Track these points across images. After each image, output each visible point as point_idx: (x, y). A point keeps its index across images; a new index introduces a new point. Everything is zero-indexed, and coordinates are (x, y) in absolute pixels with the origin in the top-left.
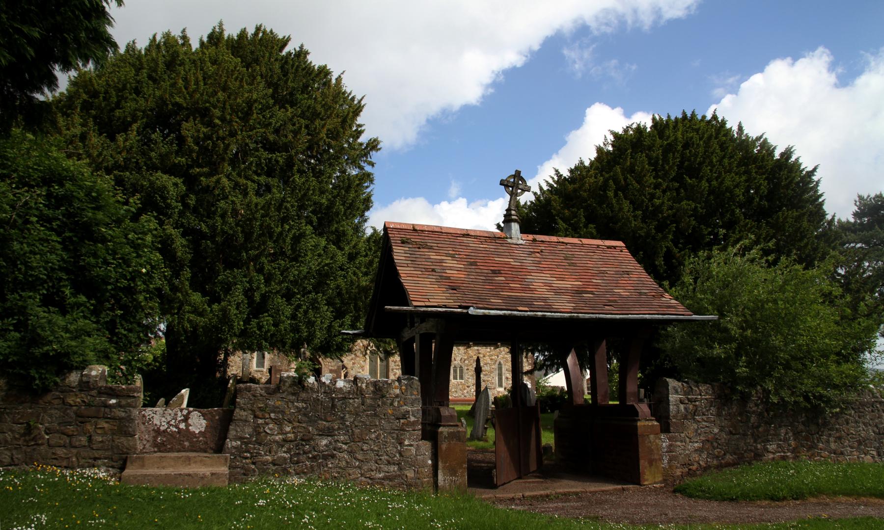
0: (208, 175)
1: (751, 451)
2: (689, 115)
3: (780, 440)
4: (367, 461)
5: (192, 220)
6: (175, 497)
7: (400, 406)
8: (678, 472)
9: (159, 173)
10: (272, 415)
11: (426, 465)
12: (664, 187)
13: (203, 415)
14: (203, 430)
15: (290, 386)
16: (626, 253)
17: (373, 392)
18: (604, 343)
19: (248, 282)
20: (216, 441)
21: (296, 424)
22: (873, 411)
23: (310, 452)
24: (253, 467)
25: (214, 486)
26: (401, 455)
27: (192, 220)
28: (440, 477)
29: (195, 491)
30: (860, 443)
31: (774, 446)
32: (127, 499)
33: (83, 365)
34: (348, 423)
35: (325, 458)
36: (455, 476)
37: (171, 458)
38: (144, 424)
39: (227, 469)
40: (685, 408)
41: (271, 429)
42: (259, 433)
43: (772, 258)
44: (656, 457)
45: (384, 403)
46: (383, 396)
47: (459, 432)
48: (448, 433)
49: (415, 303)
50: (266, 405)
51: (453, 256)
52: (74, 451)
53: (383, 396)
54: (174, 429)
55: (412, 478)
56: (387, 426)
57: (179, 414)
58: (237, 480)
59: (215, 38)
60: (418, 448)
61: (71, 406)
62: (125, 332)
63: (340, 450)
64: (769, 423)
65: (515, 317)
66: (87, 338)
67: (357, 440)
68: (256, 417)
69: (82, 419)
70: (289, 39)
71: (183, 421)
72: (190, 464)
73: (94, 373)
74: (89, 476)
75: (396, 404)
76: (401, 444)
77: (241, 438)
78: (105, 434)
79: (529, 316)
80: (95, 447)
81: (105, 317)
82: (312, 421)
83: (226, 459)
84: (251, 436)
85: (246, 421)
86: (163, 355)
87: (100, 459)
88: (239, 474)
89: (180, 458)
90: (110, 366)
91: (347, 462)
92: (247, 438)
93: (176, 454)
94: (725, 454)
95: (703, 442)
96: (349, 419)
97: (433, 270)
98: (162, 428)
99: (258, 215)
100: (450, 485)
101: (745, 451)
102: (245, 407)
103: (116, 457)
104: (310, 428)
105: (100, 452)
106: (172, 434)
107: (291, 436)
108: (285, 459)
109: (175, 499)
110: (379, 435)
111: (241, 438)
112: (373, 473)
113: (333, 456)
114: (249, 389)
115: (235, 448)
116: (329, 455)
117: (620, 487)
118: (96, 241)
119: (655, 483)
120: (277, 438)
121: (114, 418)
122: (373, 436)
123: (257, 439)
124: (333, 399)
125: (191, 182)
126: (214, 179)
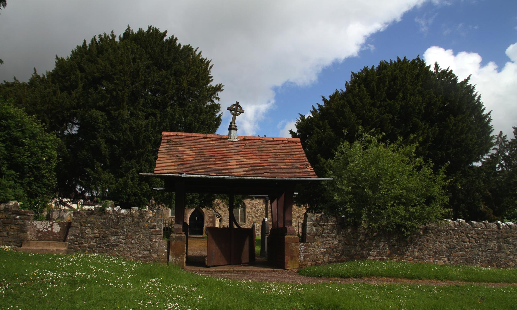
0: (115, 110)
1: (359, 254)
2: (402, 60)
3: (379, 249)
4: (134, 248)
7: (151, 222)
8: (309, 264)
9: (94, 110)
10: (89, 225)
11: (163, 252)
12: (378, 105)
15: (98, 212)
16: (300, 145)
17: (139, 215)
19: (139, 166)
22: (446, 235)
23: (106, 243)
28: (170, 258)
30: (435, 253)
31: (375, 253)
35: (113, 246)
40: (316, 230)
41: (88, 231)
42: (82, 233)
43: (100, 146)
44: (295, 255)
45: (143, 221)
46: (143, 218)
49: (155, 172)
51: (191, 149)
53: (143, 218)
55: (156, 258)
56: (145, 232)
59: (127, 34)
60: (160, 243)
63: (121, 242)
64: (372, 239)
65: (207, 178)
68: (82, 226)
70: (166, 32)
71: (50, 227)
73: (11, 204)
75: (149, 221)
76: (151, 241)
78: (14, 231)
79: (215, 178)
80: (10, 237)
81: (26, 180)
82: (107, 228)
83: (66, 244)
84: (79, 234)
85: (77, 227)
94: (341, 256)
96: (126, 228)
97: (177, 156)
99: (142, 131)
100: (175, 262)
101: (355, 255)
106: (45, 233)
107: (97, 235)
108: (94, 245)
110: (140, 236)
111: (74, 235)
113: (117, 245)
116: (115, 245)
118: (19, 145)
121: (18, 224)
124: (118, 218)
125: (108, 113)
126: (117, 112)
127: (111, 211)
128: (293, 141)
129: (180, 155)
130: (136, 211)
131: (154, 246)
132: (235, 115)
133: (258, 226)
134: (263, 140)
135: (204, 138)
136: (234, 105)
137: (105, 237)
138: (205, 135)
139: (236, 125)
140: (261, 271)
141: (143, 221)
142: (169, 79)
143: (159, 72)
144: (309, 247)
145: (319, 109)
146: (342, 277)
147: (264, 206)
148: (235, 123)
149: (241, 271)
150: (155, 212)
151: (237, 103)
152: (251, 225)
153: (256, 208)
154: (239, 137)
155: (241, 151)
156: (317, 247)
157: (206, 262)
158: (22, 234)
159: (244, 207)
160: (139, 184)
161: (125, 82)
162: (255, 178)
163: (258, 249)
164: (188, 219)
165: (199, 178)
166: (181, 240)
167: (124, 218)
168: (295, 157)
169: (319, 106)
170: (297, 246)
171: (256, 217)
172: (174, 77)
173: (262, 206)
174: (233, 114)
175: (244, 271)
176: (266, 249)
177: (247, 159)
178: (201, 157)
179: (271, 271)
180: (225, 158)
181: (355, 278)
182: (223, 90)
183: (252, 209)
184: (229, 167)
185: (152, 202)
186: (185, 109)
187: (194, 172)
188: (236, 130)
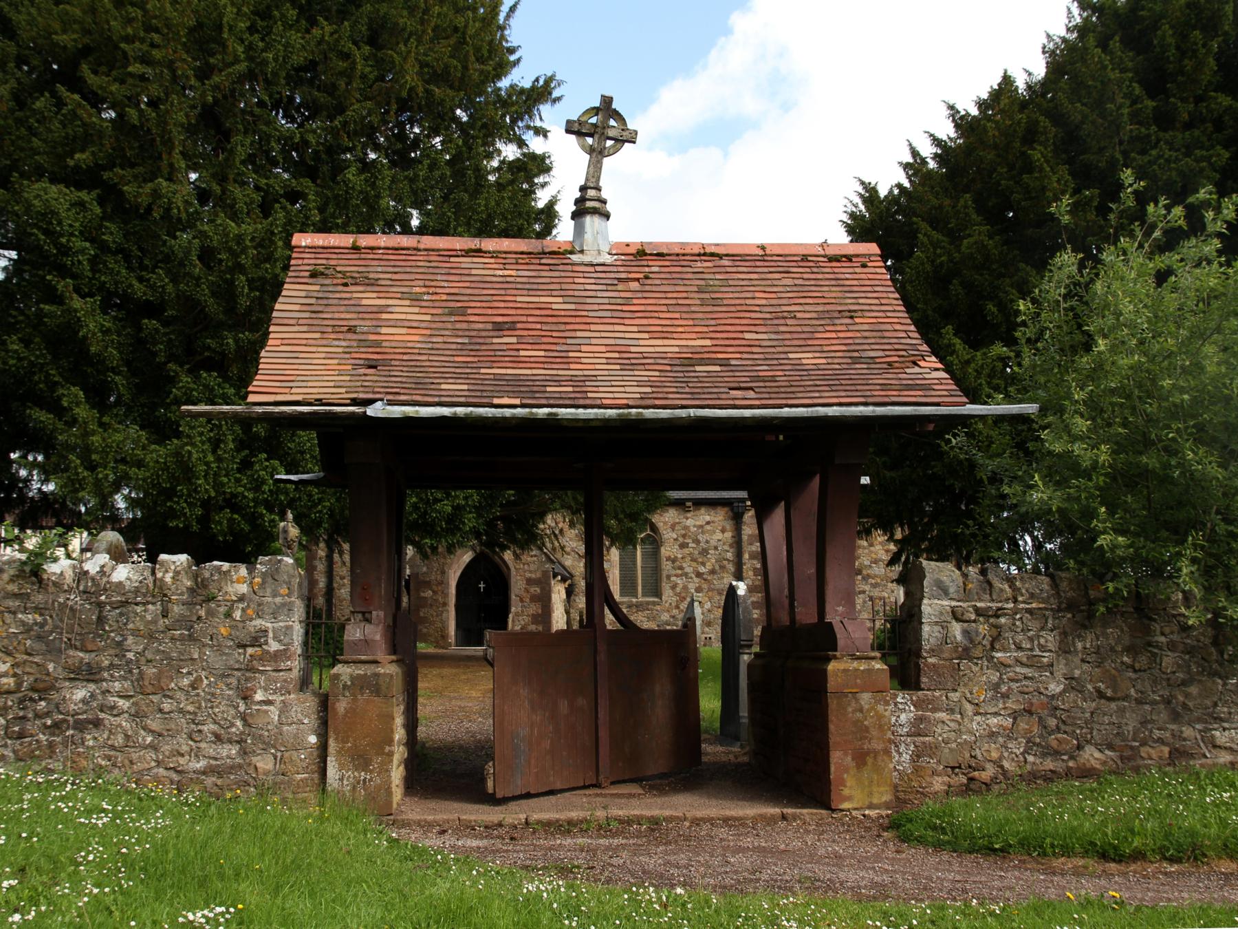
5: (119, 273)
8: (938, 784)
15: (12, 581)
16: (880, 272)
17: (191, 591)
18: (816, 481)
21: (21, 657)
23: (48, 714)
26: (246, 724)
27: (119, 273)
28: (332, 772)
34: (130, 655)
35: (80, 726)
36: (366, 769)
40: (966, 633)
44: (877, 745)
45: (211, 613)
47: (377, 675)
48: (352, 678)
49: (252, 398)
51: (415, 299)
55: (267, 773)
56: (218, 662)
67: (150, 689)
75: (237, 615)
82: (53, 651)
91: (127, 737)
95: (1015, 715)
97: (351, 330)
104: (51, 667)
110: (199, 679)
112: (182, 761)
113: (97, 723)
116: (88, 721)
117: (774, 811)
119: (871, 807)
122: (186, 682)
124: (100, 605)
125: (111, 196)
127: (69, 575)
128: (849, 258)
129: (364, 325)
130: (177, 573)
131: (259, 721)
132: (597, 155)
133: (706, 613)
134: (720, 257)
135: (468, 253)
136: (595, 111)
137: (43, 688)
138: (474, 243)
139: (604, 194)
140: (726, 820)
141: (211, 613)
142: (346, 56)
143: (308, 31)
144: (934, 710)
145: (936, 156)
146: (1104, 856)
147: (729, 535)
148: (599, 189)
149: (639, 820)
150: (264, 575)
151: (607, 101)
152: (684, 606)
153: (697, 542)
154: (617, 245)
155: (627, 301)
156: (969, 708)
157: (490, 784)
159: (655, 542)
160: (246, 465)
161: (171, 65)
162: (692, 412)
163: (710, 703)
164: (453, 590)
165: (443, 418)
166: (377, 691)
167: (125, 603)
168: (863, 323)
169: (937, 142)
170: (880, 708)
171: (699, 575)
172: (367, 49)
173: (719, 536)
174: (591, 151)
175: (655, 822)
176: (744, 712)
177: (653, 335)
178: (456, 333)
179: (770, 821)
180: (557, 332)
181: (1172, 860)
182: (559, 99)
183: (683, 546)
184: (575, 371)
185: (285, 531)
186: (416, 175)
187: (422, 389)
188: (607, 216)
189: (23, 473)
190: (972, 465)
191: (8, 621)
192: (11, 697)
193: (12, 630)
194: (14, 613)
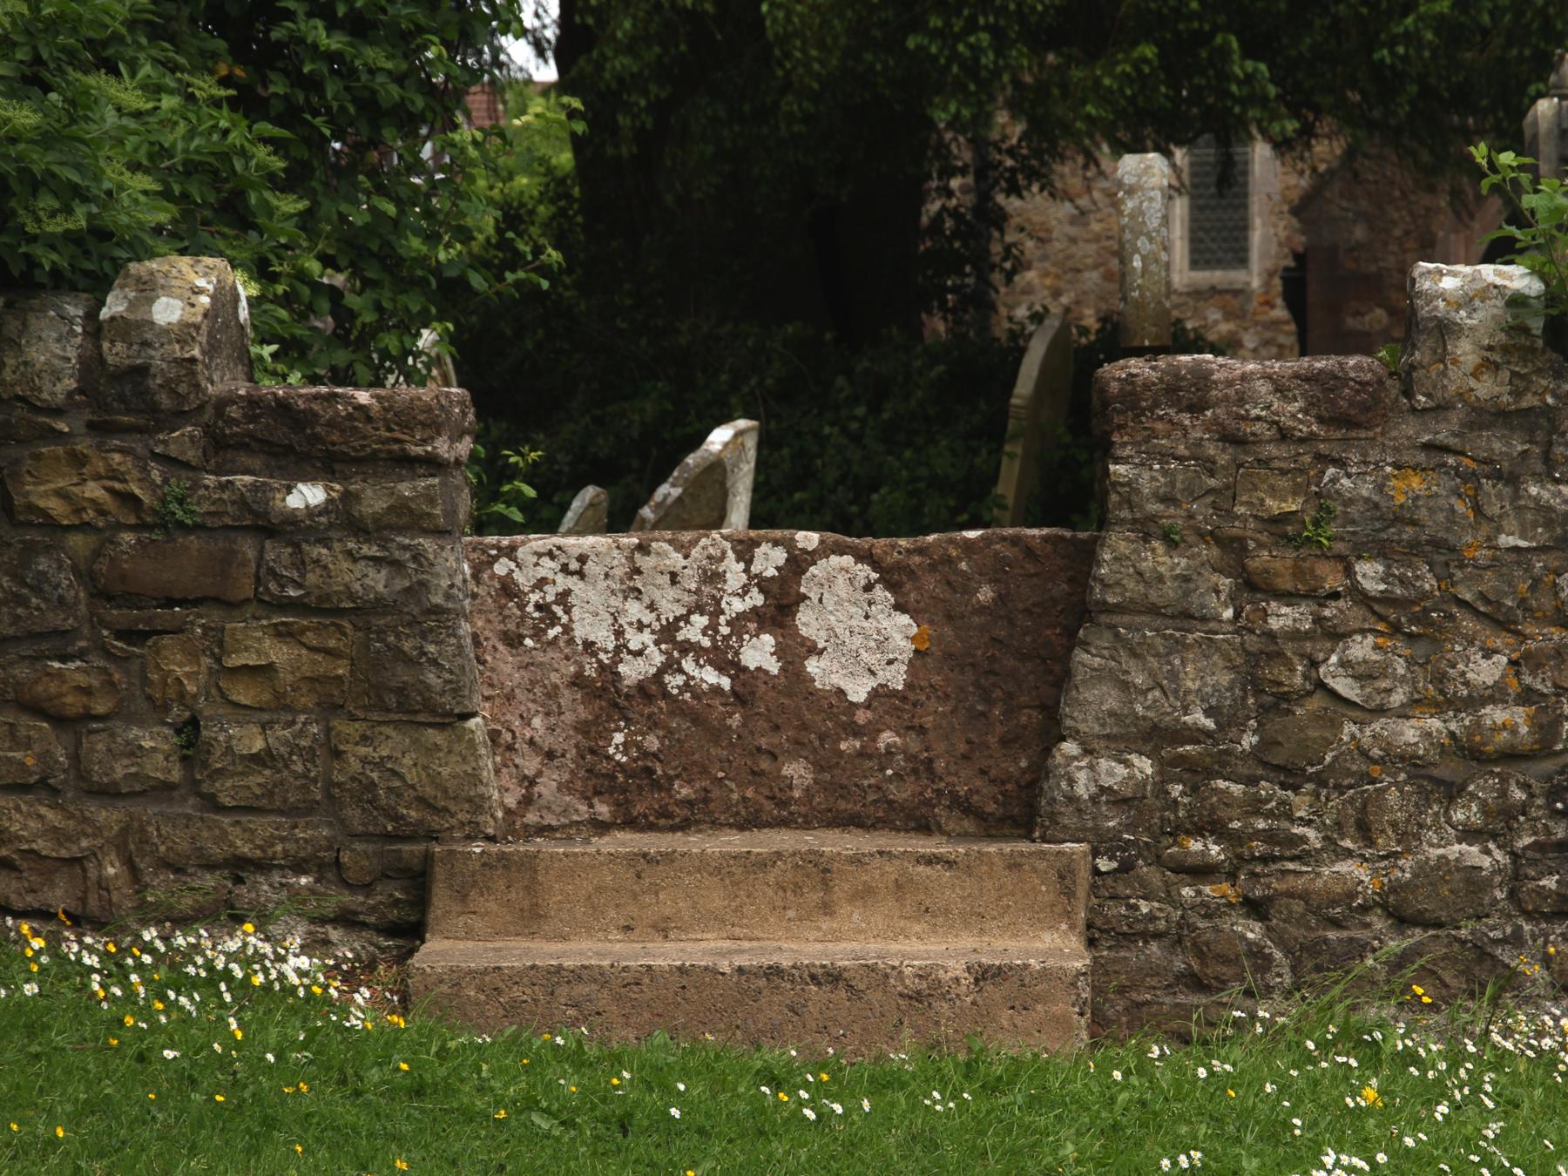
6: (758, 1108)
10: (1370, 574)
13: (892, 577)
14: (896, 678)
20: (976, 762)
24: (1253, 932)
25: (1005, 1047)
29: (884, 1083)
32: (469, 1116)
33: (98, 259)
37: (702, 862)
38: (513, 641)
39: (1075, 943)
41: (1365, 674)
50: (1324, 505)
52: (108, 816)
54: (710, 676)
57: (734, 573)
58: (1140, 1018)
61: (50, 524)
62: (333, 42)
66: (98, 81)
68: (1253, 587)
69: (132, 613)
72: (827, 909)
73: (167, 311)
74: (215, 976)
77: (1155, 736)
78: (280, 707)
83: (1065, 875)
84: (1228, 721)
85: (1186, 617)
86: (556, 188)
87: (262, 866)
88: (1154, 980)
89: (763, 864)
90: (261, 271)
92: (1196, 735)
93: (733, 842)
98: (632, 671)
102: (1173, 517)
103: (357, 856)
105: (263, 826)
106: (696, 710)
107: (1508, 720)
109: (761, 1125)
111: (1155, 736)
114: (1192, 395)
115: (1120, 801)
120: (1409, 733)
121: (322, 608)
123: (1266, 744)
158: (392, 744)
189: (579, 219)
190: (841, 692)
191: (1494, 509)
192: (1517, 772)
193: (1506, 540)
194: (1513, 480)
